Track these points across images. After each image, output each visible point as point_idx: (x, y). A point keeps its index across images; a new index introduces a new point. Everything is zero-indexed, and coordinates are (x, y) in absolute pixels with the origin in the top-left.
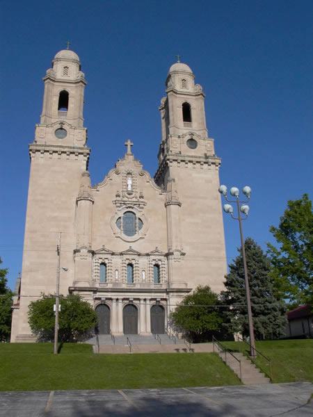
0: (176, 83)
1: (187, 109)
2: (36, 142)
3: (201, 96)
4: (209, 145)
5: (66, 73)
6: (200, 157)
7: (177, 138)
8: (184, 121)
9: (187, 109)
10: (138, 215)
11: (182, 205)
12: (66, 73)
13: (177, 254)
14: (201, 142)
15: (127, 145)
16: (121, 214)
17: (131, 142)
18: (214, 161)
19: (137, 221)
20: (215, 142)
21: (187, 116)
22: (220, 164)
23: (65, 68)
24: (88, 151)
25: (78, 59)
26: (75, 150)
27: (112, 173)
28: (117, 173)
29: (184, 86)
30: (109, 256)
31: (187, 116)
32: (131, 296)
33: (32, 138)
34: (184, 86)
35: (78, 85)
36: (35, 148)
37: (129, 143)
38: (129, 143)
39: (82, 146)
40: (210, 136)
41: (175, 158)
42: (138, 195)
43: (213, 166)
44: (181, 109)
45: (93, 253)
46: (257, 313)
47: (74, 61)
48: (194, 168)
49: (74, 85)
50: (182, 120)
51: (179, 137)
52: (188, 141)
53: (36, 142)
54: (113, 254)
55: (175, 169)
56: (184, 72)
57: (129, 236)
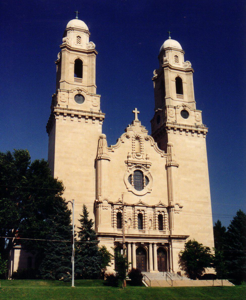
0: (169, 58)
1: (78, 65)
2: (59, 105)
3: (94, 54)
4: (198, 116)
5: (79, 43)
6: (191, 126)
7: (173, 109)
8: (75, 76)
9: (78, 65)
10: (145, 173)
11: (180, 167)
12: (79, 43)
13: (177, 207)
14: (192, 113)
15: (135, 113)
16: (132, 172)
17: (138, 110)
18: (202, 130)
19: (144, 178)
20: (202, 113)
21: (179, 90)
22: (103, 119)
23: (77, 37)
24: (103, 116)
25: (87, 29)
26: (93, 115)
27: (123, 137)
28: (128, 137)
29: (177, 61)
30: (144, 208)
31: (179, 90)
32: (142, 241)
33: (54, 102)
34: (177, 61)
35: (188, 73)
36: (59, 111)
37: (136, 111)
38: (136, 111)
39: (98, 112)
40: (98, 92)
41: (172, 126)
42: (144, 157)
43: (97, 121)
44: (175, 83)
45: (112, 204)
46: (102, 267)
47: (86, 32)
48: (72, 121)
49: (185, 73)
50: (73, 74)
51: (175, 108)
52: (76, 95)
53: (59, 105)
54: (147, 207)
55: (172, 137)
56: (177, 50)
57: (138, 190)
